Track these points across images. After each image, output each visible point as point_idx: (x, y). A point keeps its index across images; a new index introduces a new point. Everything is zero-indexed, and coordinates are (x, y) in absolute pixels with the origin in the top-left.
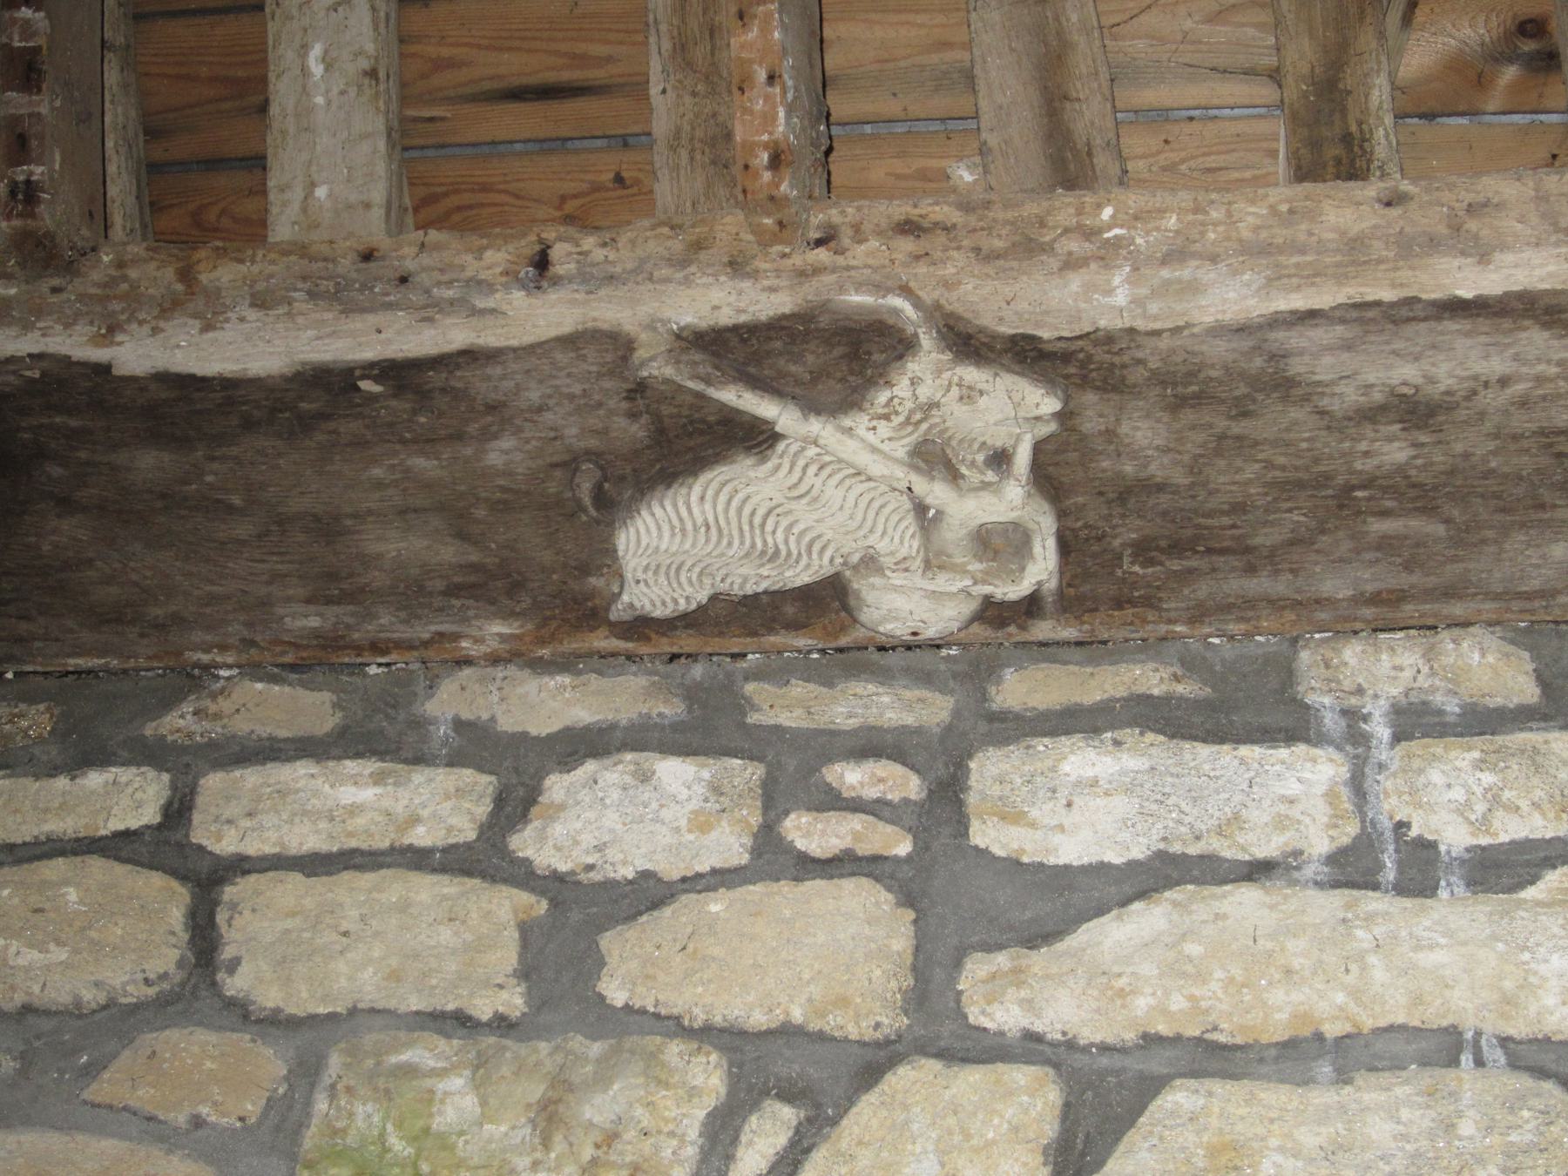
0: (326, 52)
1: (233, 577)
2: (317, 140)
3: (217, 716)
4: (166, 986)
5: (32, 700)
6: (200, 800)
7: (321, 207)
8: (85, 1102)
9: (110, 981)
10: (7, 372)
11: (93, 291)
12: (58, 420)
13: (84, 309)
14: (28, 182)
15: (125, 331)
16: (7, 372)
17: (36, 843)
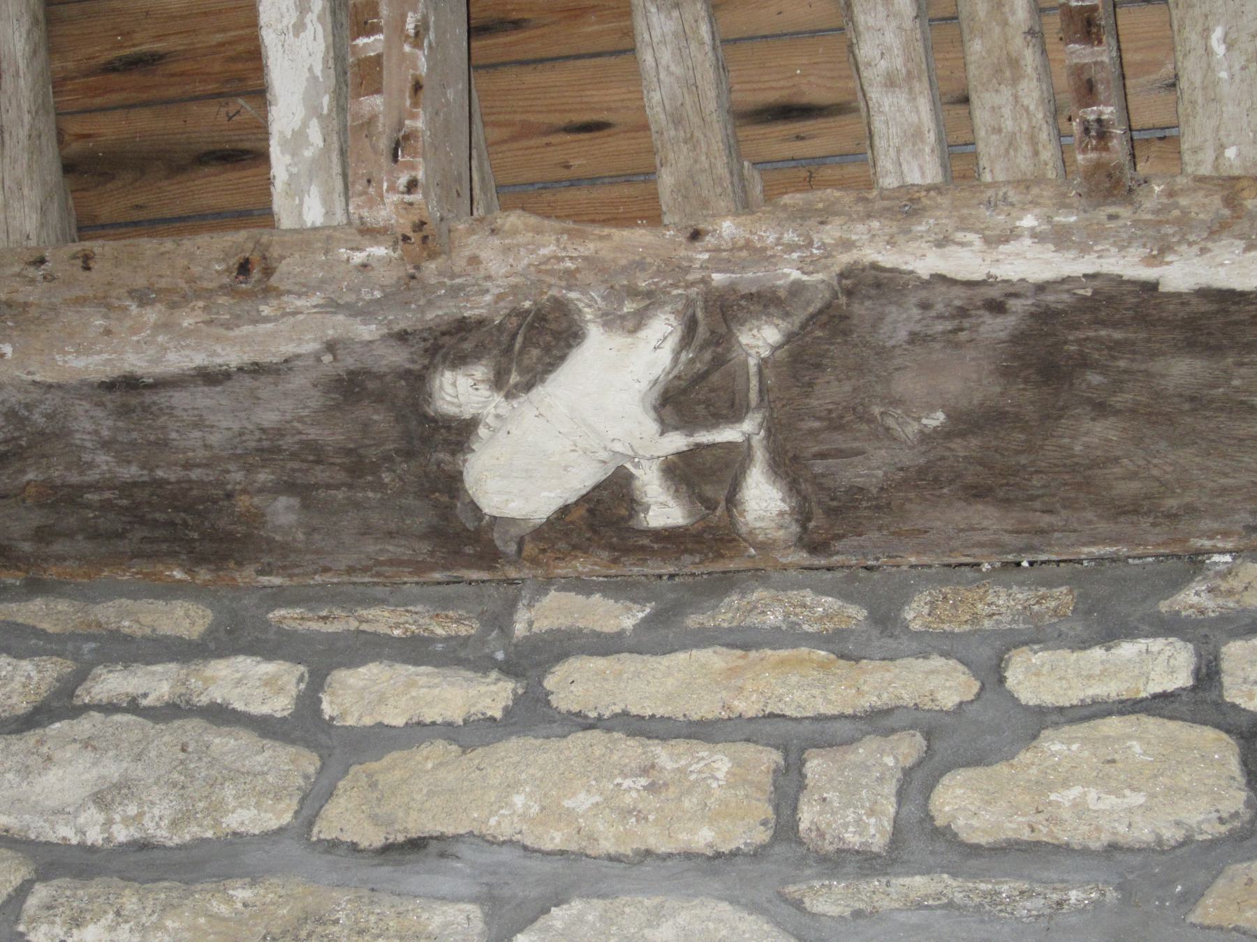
0: (1226, 35)
1: (1247, 470)
2: (1224, 109)
3: (1230, 592)
4: (1237, 824)
5: (1050, 584)
6: (1225, 665)
7: (1231, 166)
8: (1193, 925)
9: (1188, 821)
10: (1062, 291)
11: (1149, 217)
12: (1103, 333)
13: (1139, 233)
14: (1099, 121)
15: (1175, 252)
16: (1062, 291)
17: (1083, 705)
